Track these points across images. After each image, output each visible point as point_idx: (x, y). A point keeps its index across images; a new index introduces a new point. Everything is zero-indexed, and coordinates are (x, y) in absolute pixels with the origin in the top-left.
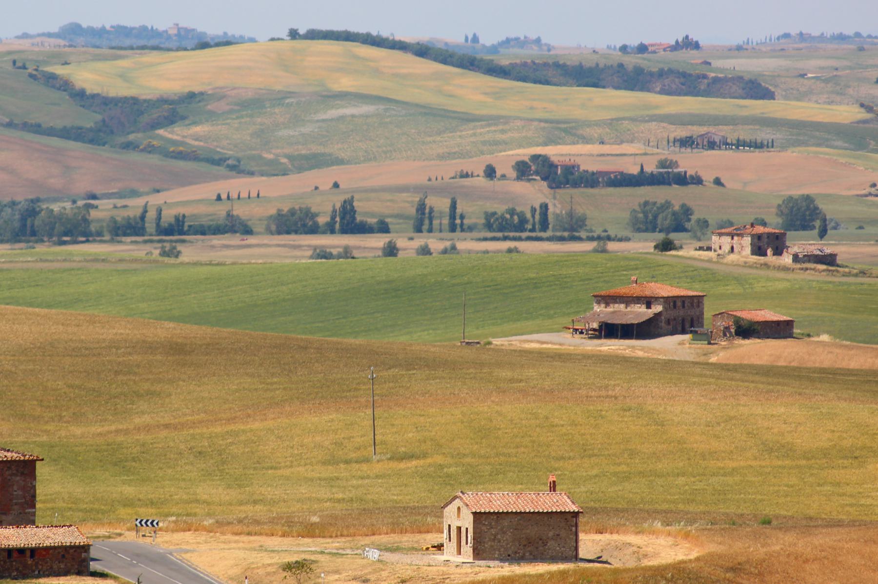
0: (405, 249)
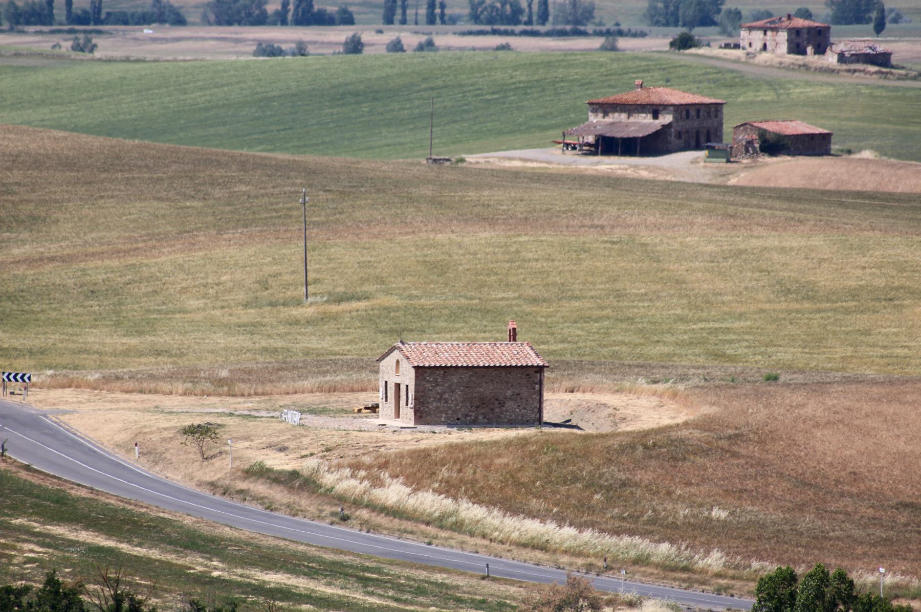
0: (372, 45)
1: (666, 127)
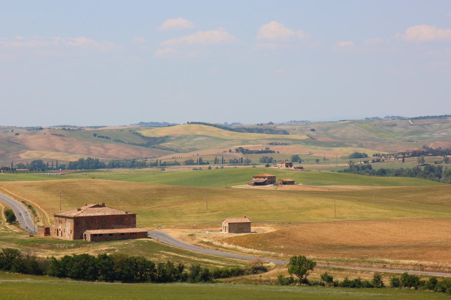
1: (266, 180)
